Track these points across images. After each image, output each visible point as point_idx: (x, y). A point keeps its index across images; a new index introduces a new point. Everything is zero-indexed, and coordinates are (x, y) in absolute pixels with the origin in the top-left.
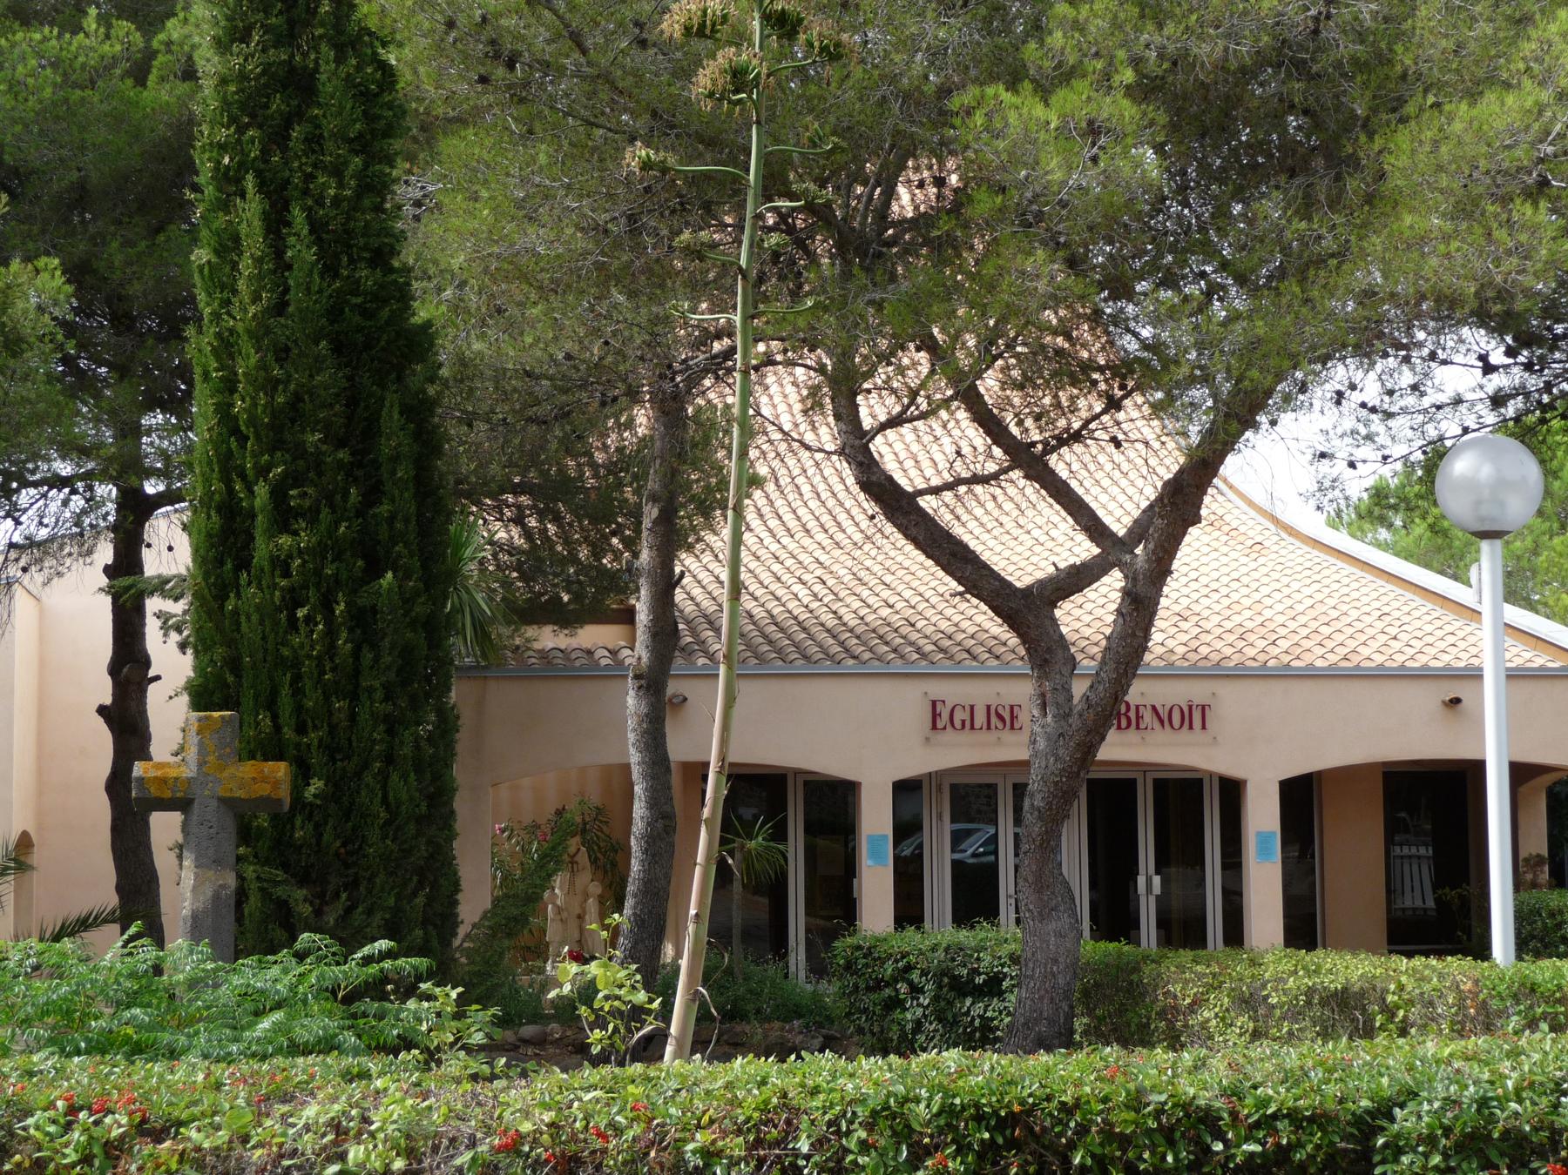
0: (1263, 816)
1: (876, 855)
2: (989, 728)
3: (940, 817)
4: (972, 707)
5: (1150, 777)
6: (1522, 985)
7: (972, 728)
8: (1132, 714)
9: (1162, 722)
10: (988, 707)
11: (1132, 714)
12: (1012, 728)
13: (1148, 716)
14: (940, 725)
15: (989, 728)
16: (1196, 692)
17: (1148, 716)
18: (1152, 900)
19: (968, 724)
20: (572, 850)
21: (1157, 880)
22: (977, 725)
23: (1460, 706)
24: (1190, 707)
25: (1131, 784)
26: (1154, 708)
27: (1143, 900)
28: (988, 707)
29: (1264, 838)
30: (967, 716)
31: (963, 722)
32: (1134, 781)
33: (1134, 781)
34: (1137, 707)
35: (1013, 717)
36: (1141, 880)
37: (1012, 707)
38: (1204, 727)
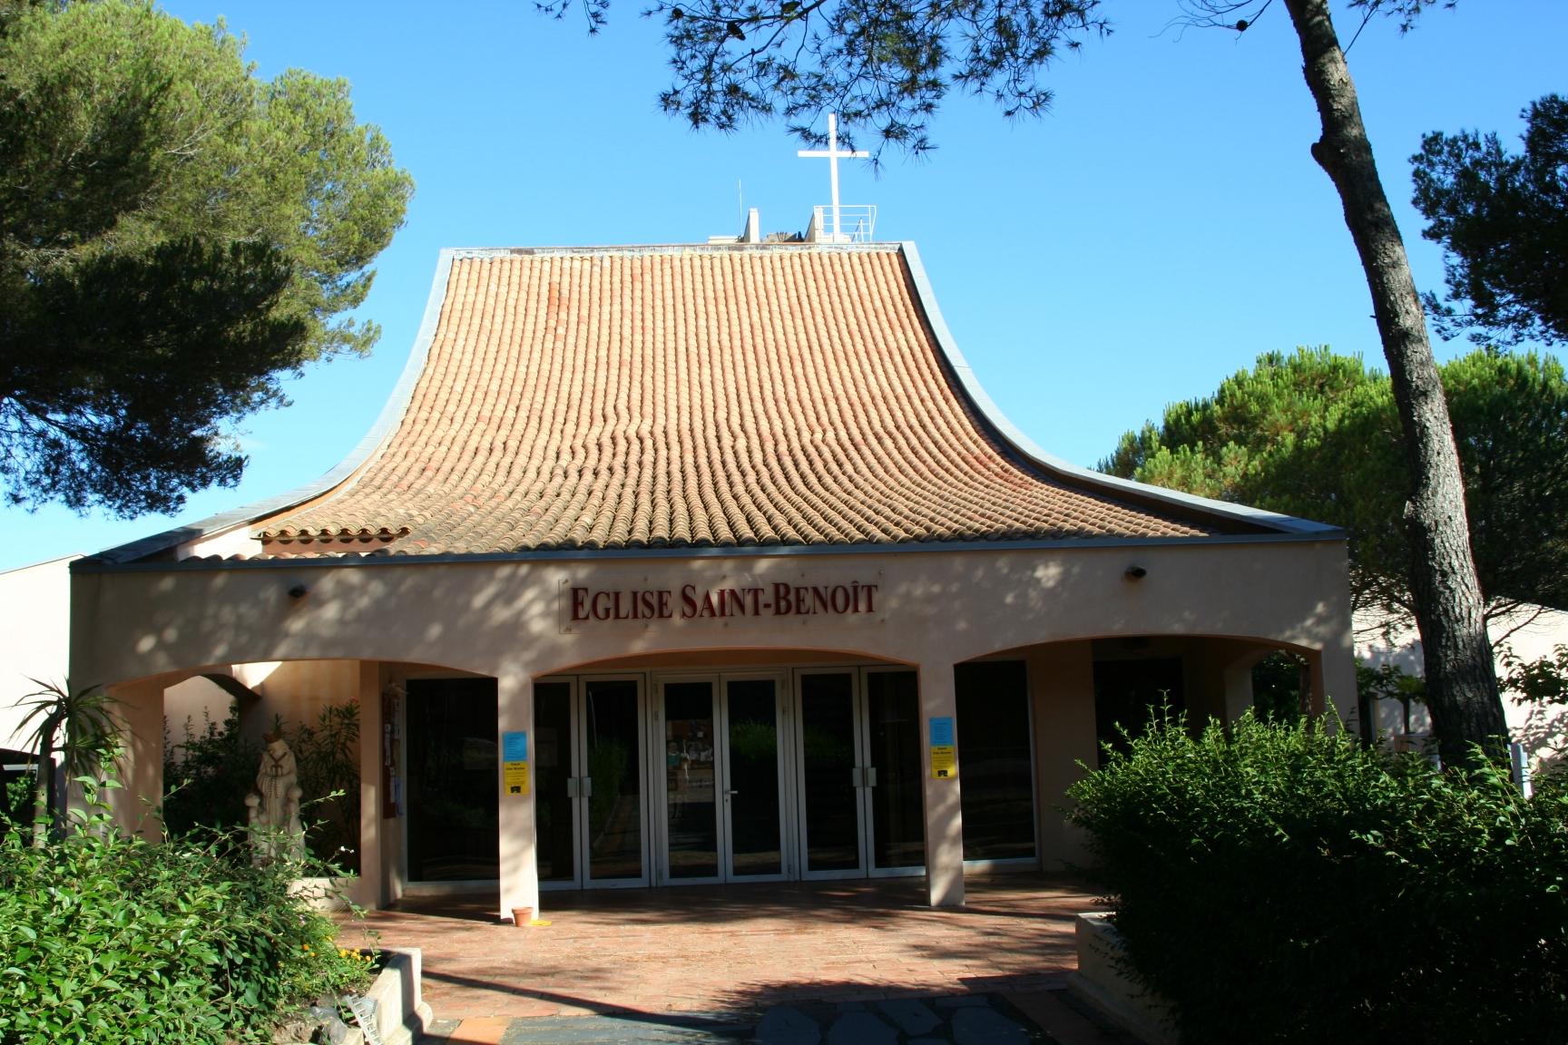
0: (938, 702)
1: (939, 738)
2: (635, 616)
3: (656, 717)
4: (617, 595)
5: (864, 672)
6: (1259, 362)
7: (617, 616)
8: (792, 597)
9: (825, 606)
10: (635, 594)
11: (792, 597)
12: (661, 615)
13: (809, 599)
14: (582, 614)
15: (635, 616)
16: (862, 572)
17: (809, 599)
18: (869, 791)
19: (612, 613)
20: (279, 753)
21: (872, 773)
22: (623, 613)
23: (1145, 578)
24: (855, 588)
25: (845, 679)
26: (816, 590)
27: (859, 792)
28: (635, 594)
29: (939, 726)
30: (611, 604)
31: (607, 610)
32: (848, 676)
33: (848, 676)
34: (798, 590)
35: (662, 604)
36: (857, 773)
37: (661, 594)
38: (870, 609)
